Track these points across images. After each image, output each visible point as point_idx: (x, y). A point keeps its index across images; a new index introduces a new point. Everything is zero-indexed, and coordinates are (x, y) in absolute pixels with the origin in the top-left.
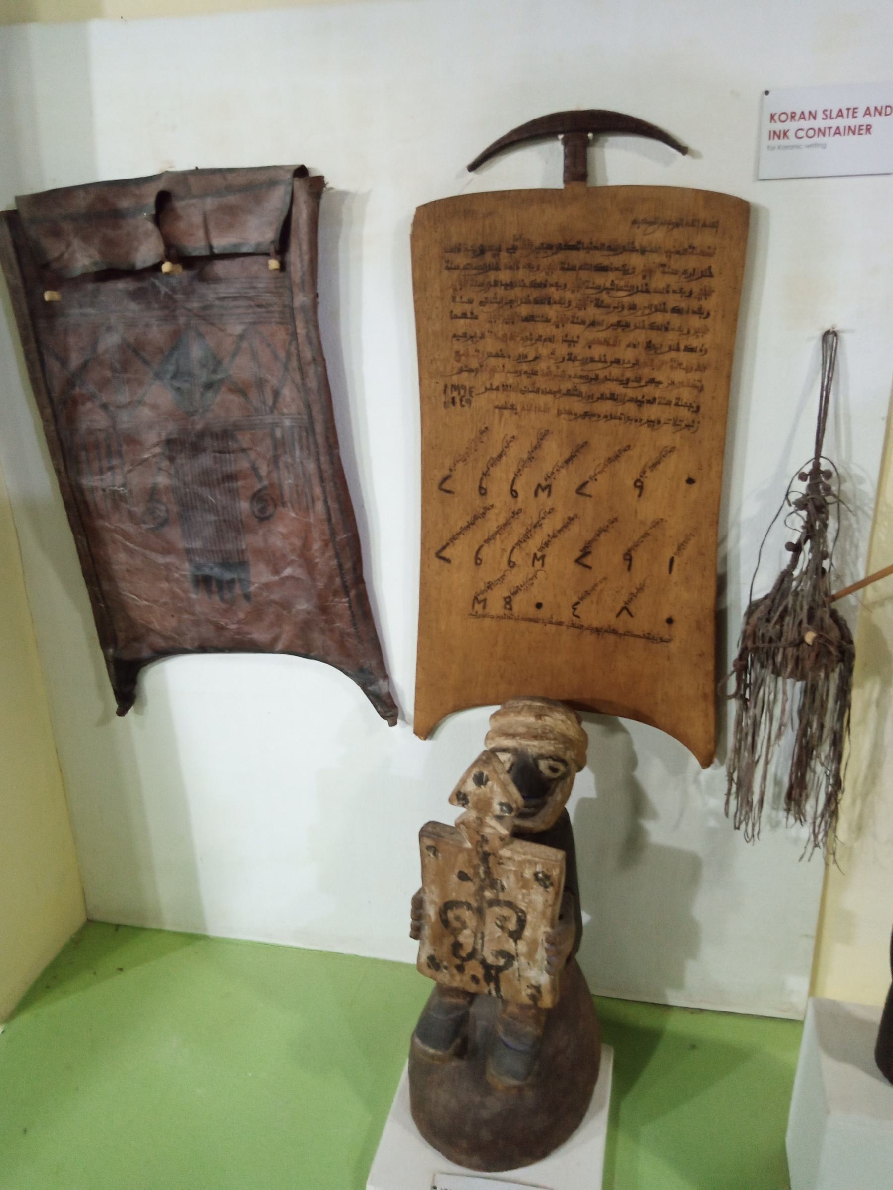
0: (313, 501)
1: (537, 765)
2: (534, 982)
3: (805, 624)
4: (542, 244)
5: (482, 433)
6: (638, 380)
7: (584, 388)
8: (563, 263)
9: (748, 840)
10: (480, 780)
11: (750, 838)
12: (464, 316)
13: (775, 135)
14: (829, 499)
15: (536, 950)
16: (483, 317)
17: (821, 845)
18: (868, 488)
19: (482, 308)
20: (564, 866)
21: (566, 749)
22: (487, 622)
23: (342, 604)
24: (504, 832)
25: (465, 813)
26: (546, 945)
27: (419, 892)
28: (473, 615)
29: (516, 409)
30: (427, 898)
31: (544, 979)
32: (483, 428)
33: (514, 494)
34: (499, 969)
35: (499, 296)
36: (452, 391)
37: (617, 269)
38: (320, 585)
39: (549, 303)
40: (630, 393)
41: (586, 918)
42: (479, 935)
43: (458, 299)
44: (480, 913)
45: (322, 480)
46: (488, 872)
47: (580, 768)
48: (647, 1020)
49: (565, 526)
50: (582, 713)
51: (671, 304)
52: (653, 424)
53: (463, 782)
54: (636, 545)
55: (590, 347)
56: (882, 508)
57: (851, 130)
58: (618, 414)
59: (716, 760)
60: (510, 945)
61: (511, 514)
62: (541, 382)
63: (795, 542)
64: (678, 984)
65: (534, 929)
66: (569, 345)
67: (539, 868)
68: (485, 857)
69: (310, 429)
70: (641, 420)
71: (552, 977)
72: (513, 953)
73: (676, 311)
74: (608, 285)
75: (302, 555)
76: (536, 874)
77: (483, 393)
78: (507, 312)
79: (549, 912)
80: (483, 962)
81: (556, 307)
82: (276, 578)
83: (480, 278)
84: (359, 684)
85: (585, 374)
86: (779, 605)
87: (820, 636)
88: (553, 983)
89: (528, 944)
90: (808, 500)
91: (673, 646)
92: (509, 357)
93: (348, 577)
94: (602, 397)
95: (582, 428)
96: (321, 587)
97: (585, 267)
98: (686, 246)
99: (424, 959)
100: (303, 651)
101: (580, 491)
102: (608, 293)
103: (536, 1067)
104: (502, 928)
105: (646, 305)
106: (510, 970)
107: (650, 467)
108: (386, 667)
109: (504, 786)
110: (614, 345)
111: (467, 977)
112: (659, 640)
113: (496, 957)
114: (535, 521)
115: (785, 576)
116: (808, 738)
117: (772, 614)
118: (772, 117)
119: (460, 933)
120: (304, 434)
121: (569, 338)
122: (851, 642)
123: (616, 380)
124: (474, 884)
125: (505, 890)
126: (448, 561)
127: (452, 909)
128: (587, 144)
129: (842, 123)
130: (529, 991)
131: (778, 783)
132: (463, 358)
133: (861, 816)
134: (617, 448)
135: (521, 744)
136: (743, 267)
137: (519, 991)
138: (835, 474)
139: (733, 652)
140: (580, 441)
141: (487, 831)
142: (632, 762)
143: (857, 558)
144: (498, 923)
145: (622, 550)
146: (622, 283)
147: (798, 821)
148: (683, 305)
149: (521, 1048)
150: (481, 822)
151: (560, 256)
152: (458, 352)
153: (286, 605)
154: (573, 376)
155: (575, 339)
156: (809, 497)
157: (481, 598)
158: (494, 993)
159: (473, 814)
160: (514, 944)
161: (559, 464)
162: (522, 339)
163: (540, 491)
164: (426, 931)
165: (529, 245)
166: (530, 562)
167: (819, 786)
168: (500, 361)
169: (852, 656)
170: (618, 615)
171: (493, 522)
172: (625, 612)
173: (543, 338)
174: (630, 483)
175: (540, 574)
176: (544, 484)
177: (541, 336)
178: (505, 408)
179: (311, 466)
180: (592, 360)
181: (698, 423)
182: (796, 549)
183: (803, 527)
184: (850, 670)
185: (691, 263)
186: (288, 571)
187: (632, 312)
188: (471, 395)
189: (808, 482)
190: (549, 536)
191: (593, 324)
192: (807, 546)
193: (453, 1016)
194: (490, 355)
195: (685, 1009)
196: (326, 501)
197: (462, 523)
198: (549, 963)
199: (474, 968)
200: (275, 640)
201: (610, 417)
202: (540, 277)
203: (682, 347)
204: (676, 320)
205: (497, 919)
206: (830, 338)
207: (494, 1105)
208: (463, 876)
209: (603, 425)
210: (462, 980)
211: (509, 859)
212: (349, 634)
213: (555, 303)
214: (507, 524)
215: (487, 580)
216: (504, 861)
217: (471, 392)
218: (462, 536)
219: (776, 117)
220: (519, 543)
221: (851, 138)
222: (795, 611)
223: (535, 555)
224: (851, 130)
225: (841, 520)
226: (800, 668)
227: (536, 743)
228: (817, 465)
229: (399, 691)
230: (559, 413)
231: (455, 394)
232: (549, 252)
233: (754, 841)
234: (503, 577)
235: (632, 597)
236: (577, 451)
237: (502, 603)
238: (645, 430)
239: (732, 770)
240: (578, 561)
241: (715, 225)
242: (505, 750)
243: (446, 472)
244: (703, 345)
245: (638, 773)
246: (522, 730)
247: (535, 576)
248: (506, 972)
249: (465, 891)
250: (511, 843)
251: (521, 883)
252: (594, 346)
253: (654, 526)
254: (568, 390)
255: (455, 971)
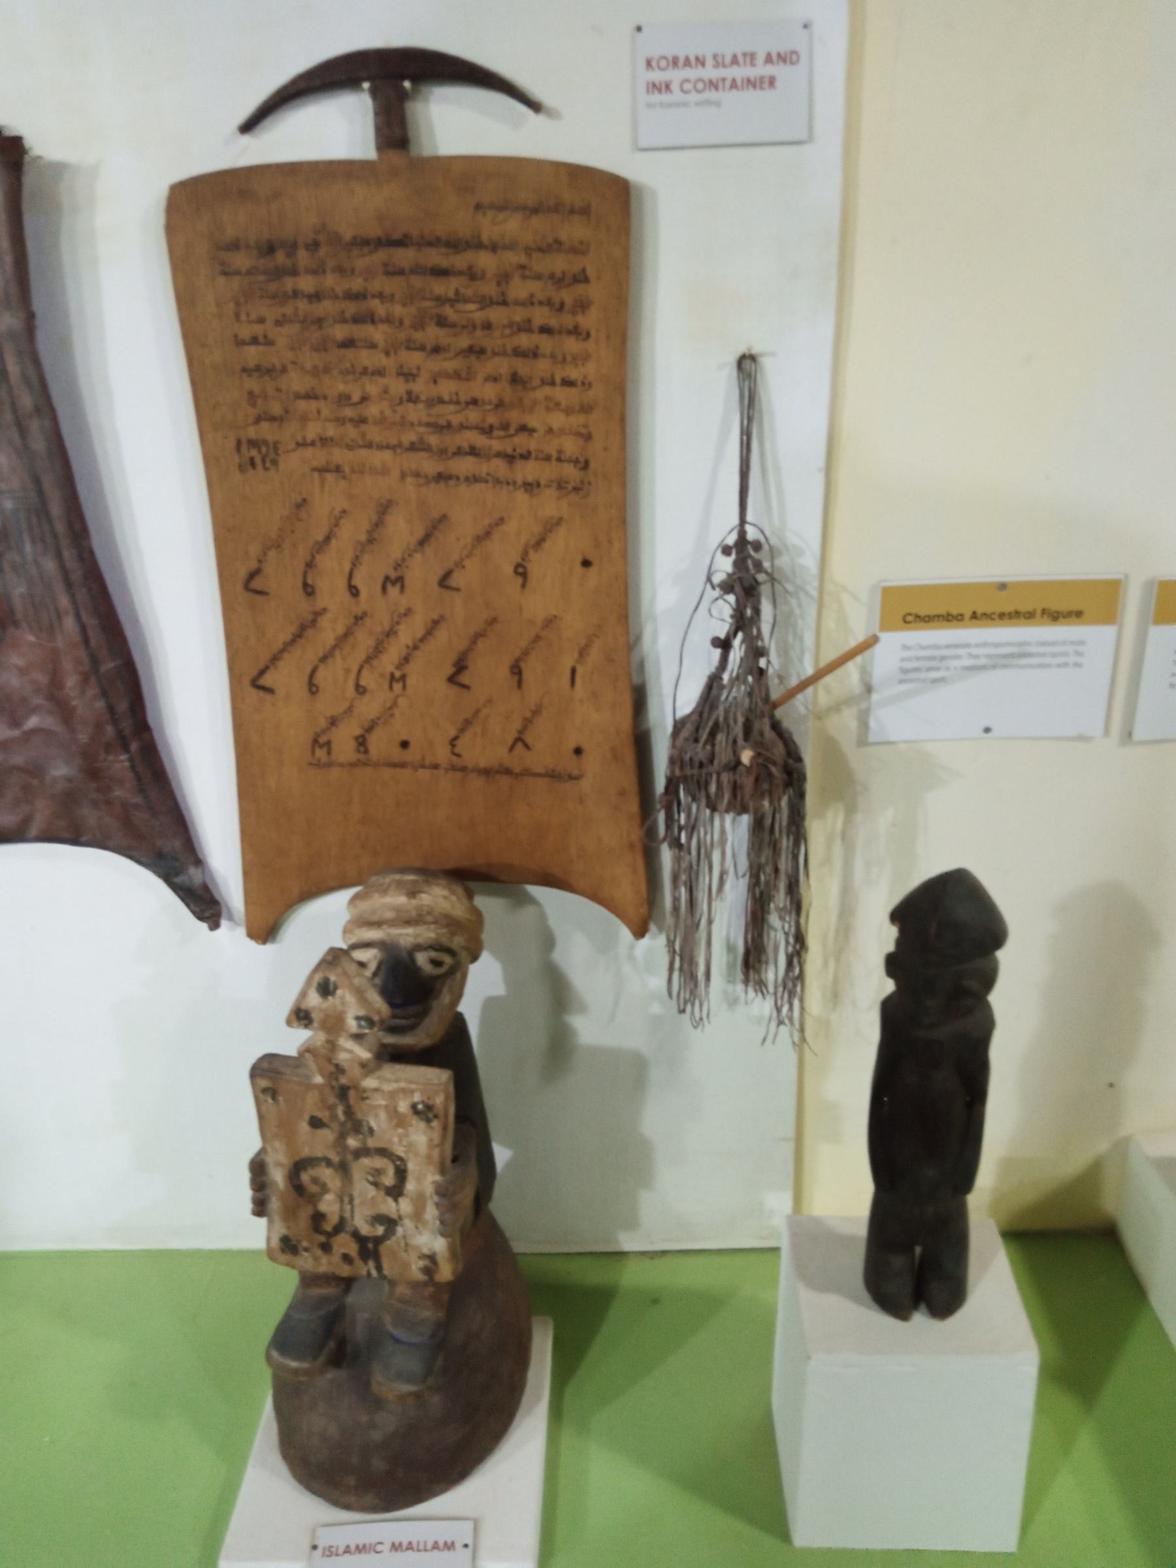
0: (59, 617)
1: (412, 959)
2: (426, 1251)
3: (740, 741)
4: (354, 238)
5: (298, 506)
6: (505, 426)
7: (433, 440)
8: (385, 265)
9: (695, 1024)
10: (326, 990)
11: (697, 1023)
12: (254, 341)
13: (654, 87)
14: (761, 577)
15: (424, 1207)
16: (281, 342)
17: (787, 1021)
18: (810, 562)
19: (279, 329)
20: (451, 1089)
21: (453, 934)
22: (335, 773)
23: (119, 764)
24: (365, 1054)
25: (310, 1039)
26: (436, 1199)
27: (259, 1153)
28: (315, 765)
29: (343, 472)
30: (270, 1159)
31: (439, 1245)
32: (299, 500)
33: (354, 591)
34: (378, 1241)
35: (301, 313)
36: (249, 449)
37: (460, 273)
38: (83, 737)
39: (373, 322)
40: (496, 445)
41: (502, 1155)
42: (346, 1199)
43: (243, 317)
44: (343, 1169)
45: (69, 585)
46: (349, 1112)
47: (475, 958)
48: (594, 1275)
49: (429, 633)
50: (472, 885)
51: (538, 321)
52: (531, 487)
53: (303, 994)
54: (526, 653)
55: (435, 382)
56: (829, 587)
57: (751, 83)
58: (484, 475)
59: (653, 927)
60: (389, 1207)
61: (352, 620)
62: (374, 433)
63: (722, 636)
64: (632, 1223)
65: (419, 1180)
66: (407, 381)
67: (417, 1097)
68: (343, 1093)
69: (42, 510)
70: (515, 483)
71: (450, 1240)
72: (394, 1216)
73: (545, 330)
74: (451, 294)
75: (51, 697)
76: (414, 1107)
77: (294, 450)
78: (315, 335)
79: (436, 1153)
80: (356, 1235)
81: (382, 327)
82: (16, 733)
83: (273, 287)
84: (159, 875)
85: (432, 420)
86: (709, 718)
87: (759, 755)
88: (452, 1249)
89: (412, 1200)
90: (735, 581)
91: (585, 784)
92: (325, 398)
93: (124, 725)
94: (459, 452)
95: (436, 495)
96: (85, 741)
97: (417, 270)
98: (550, 241)
99: (275, 1242)
100: (67, 835)
101: (444, 582)
102: (452, 306)
103: (440, 1362)
104: (375, 1184)
105: (505, 322)
106: (394, 1239)
107: (533, 547)
108: (196, 845)
109: (359, 993)
110: (468, 379)
111: (336, 1258)
112: (566, 777)
113: (373, 1225)
114: (387, 626)
115: (714, 681)
116: (762, 887)
117: (701, 730)
118: (649, 63)
119: (319, 1200)
120: (34, 520)
121: (405, 370)
122: (799, 760)
123: (476, 428)
124: (332, 1129)
125: (375, 1133)
126: (269, 690)
127: (305, 1169)
128: (403, 96)
129: (739, 73)
130: (421, 1263)
131: (730, 948)
132: (260, 402)
133: (836, 981)
134: (487, 522)
135: (389, 935)
136: (628, 269)
137: (406, 1266)
138: (766, 547)
139: (660, 784)
140: (436, 515)
141: (342, 1057)
142: (548, 941)
143: (803, 652)
144: (371, 1178)
145: (507, 661)
146: (469, 292)
147: (760, 995)
148: (553, 322)
149: (414, 1339)
150: (332, 1046)
151: (381, 255)
152: (251, 394)
153: (35, 771)
154: (416, 423)
155: (415, 371)
156: (735, 577)
157: (323, 739)
158: (374, 1273)
159: (321, 1037)
160: (394, 1204)
161: (412, 547)
162: (341, 372)
163: (389, 585)
164: (274, 1204)
165: (335, 239)
166: (386, 686)
167: (776, 948)
168: (314, 405)
169: (802, 778)
170: (512, 748)
171: (328, 632)
172: (519, 745)
173: (370, 370)
174: (509, 569)
175: (402, 701)
176: (393, 575)
177: (365, 369)
178: (327, 471)
179: (50, 565)
180: (441, 401)
181: (589, 483)
182: (724, 645)
183: (732, 617)
184: (801, 795)
185: (559, 264)
186: (33, 722)
187: (486, 332)
188: (277, 454)
189: (733, 556)
190: (408, 647)
191: (437, 350)
192: (737, 641)
193: (322, 1313)
194: (298, 396)
195: (643, 1254)
196: (78, 616)
197: (285, 636)
198: (442, 1222)
199: (344, 1244)
200: (26, 821)
201: (474, 479)
202: (357, 284)
203: (558, 380)
204: (545, 343)
205: (368, 1173)
206: (747, 365)
207: (387, 1423)
208: (316, 1123)
209: (464, 490)
210: (330, 1263)
211: (376, 1090)
212: (136, 806)
213: (382, 321)
214: (347, 634)
215: (328, 714)
216: (369, 1094)
217: (276, 449)
218: (286, 655)
219: (654, 64)
220: (369, 660)
221: (751, 94)
222: (728, 726)
223: (392, 675)
224: (751, 83)
225: (778, 602)
226: (739, 798)
227: (410, 930)
228: (742, 534)
229: (220, 881)
230: (403, 476)
231: (254, 453)
232: (366, 250)
233: (703, 1025)
234: (350, 709)
235: (527, 723)
236: (434, 527)
237: (352, 744)
238: (521, 496)
239: (672, 938)
240: (452, 680)
241: (585, 211)
242: (754, 977)
243: (253, 565)
244: (585, 377)
245: (557, 956)
246: (389, 915)
247: (395, 704)
248: (388, 1242)
249: (321, 1143)
250: (378, 1067)
251: (395, 1122)
252: (440, 381)
253: (547, 627)
254: (412, 443)
255: (319, 1252)
